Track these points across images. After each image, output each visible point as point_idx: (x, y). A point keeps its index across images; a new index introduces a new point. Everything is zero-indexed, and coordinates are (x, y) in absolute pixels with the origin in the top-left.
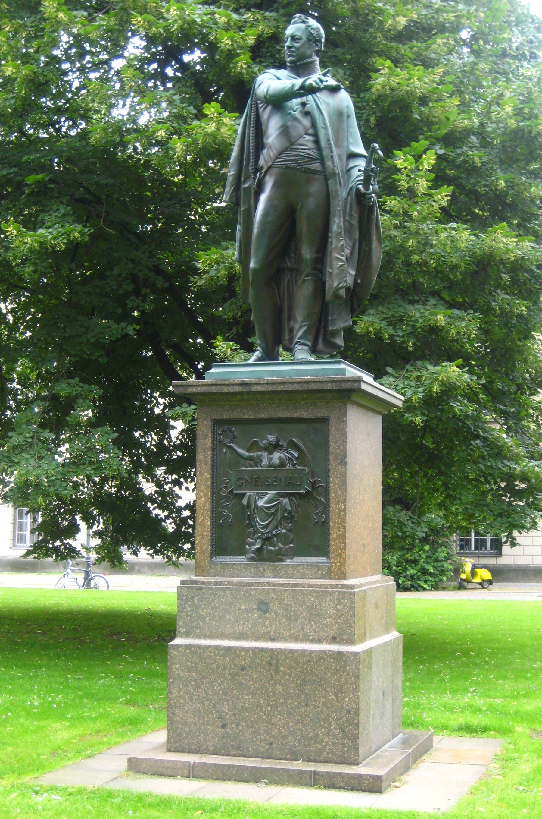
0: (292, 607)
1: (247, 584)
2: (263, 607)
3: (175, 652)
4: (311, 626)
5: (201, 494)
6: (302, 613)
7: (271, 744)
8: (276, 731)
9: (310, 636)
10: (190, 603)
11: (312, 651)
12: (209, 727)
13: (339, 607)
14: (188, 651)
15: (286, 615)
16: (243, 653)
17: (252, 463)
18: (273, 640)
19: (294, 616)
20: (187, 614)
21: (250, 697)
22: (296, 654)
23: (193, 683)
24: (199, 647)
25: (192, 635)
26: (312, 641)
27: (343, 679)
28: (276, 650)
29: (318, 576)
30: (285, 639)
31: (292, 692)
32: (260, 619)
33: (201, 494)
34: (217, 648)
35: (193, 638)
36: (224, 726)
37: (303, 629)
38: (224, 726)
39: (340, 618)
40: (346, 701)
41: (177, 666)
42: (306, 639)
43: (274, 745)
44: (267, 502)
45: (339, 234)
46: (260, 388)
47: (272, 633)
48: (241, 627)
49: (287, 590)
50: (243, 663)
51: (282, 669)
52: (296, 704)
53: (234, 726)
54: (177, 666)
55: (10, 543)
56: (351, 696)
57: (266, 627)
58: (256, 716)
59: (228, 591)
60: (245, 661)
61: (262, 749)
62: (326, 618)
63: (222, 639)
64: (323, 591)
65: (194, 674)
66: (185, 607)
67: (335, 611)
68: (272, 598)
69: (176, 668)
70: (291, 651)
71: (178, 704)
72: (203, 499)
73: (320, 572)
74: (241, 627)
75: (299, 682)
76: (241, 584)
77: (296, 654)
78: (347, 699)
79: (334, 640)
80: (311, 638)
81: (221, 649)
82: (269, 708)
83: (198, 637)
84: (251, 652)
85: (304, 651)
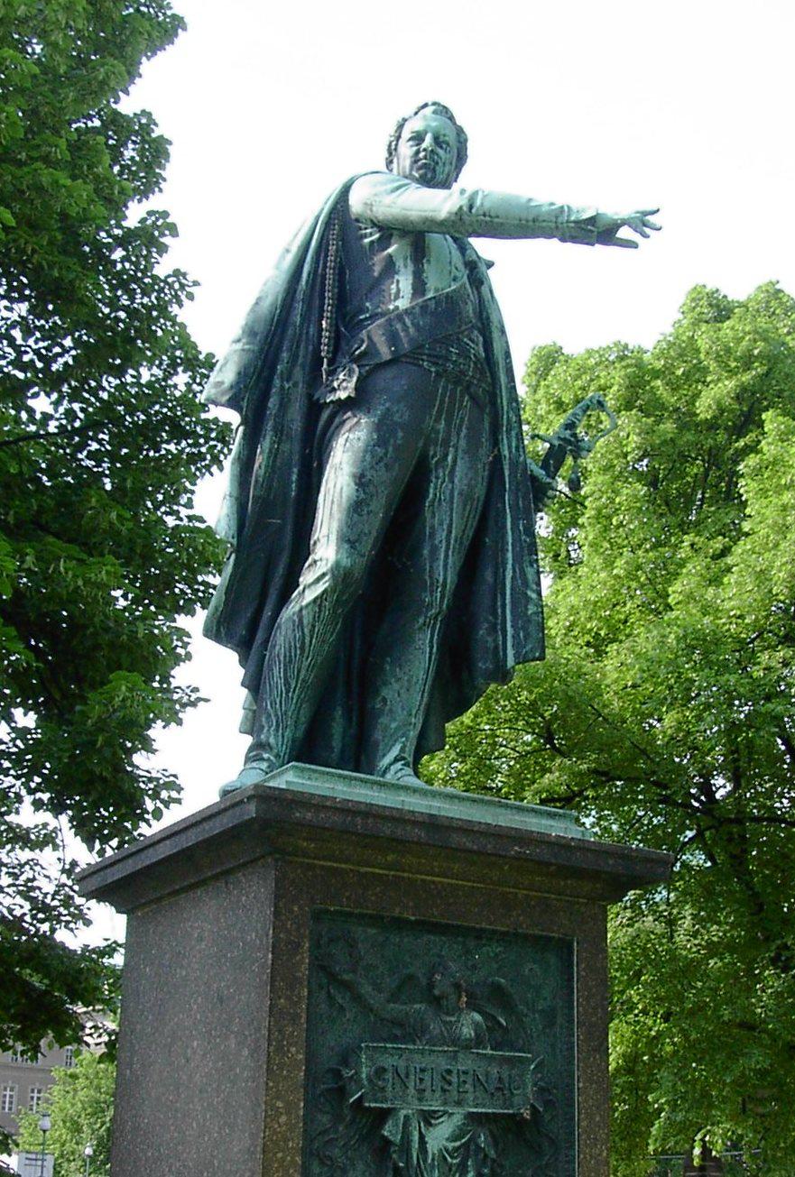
44: (453, 1138)
72: (283, 1119)
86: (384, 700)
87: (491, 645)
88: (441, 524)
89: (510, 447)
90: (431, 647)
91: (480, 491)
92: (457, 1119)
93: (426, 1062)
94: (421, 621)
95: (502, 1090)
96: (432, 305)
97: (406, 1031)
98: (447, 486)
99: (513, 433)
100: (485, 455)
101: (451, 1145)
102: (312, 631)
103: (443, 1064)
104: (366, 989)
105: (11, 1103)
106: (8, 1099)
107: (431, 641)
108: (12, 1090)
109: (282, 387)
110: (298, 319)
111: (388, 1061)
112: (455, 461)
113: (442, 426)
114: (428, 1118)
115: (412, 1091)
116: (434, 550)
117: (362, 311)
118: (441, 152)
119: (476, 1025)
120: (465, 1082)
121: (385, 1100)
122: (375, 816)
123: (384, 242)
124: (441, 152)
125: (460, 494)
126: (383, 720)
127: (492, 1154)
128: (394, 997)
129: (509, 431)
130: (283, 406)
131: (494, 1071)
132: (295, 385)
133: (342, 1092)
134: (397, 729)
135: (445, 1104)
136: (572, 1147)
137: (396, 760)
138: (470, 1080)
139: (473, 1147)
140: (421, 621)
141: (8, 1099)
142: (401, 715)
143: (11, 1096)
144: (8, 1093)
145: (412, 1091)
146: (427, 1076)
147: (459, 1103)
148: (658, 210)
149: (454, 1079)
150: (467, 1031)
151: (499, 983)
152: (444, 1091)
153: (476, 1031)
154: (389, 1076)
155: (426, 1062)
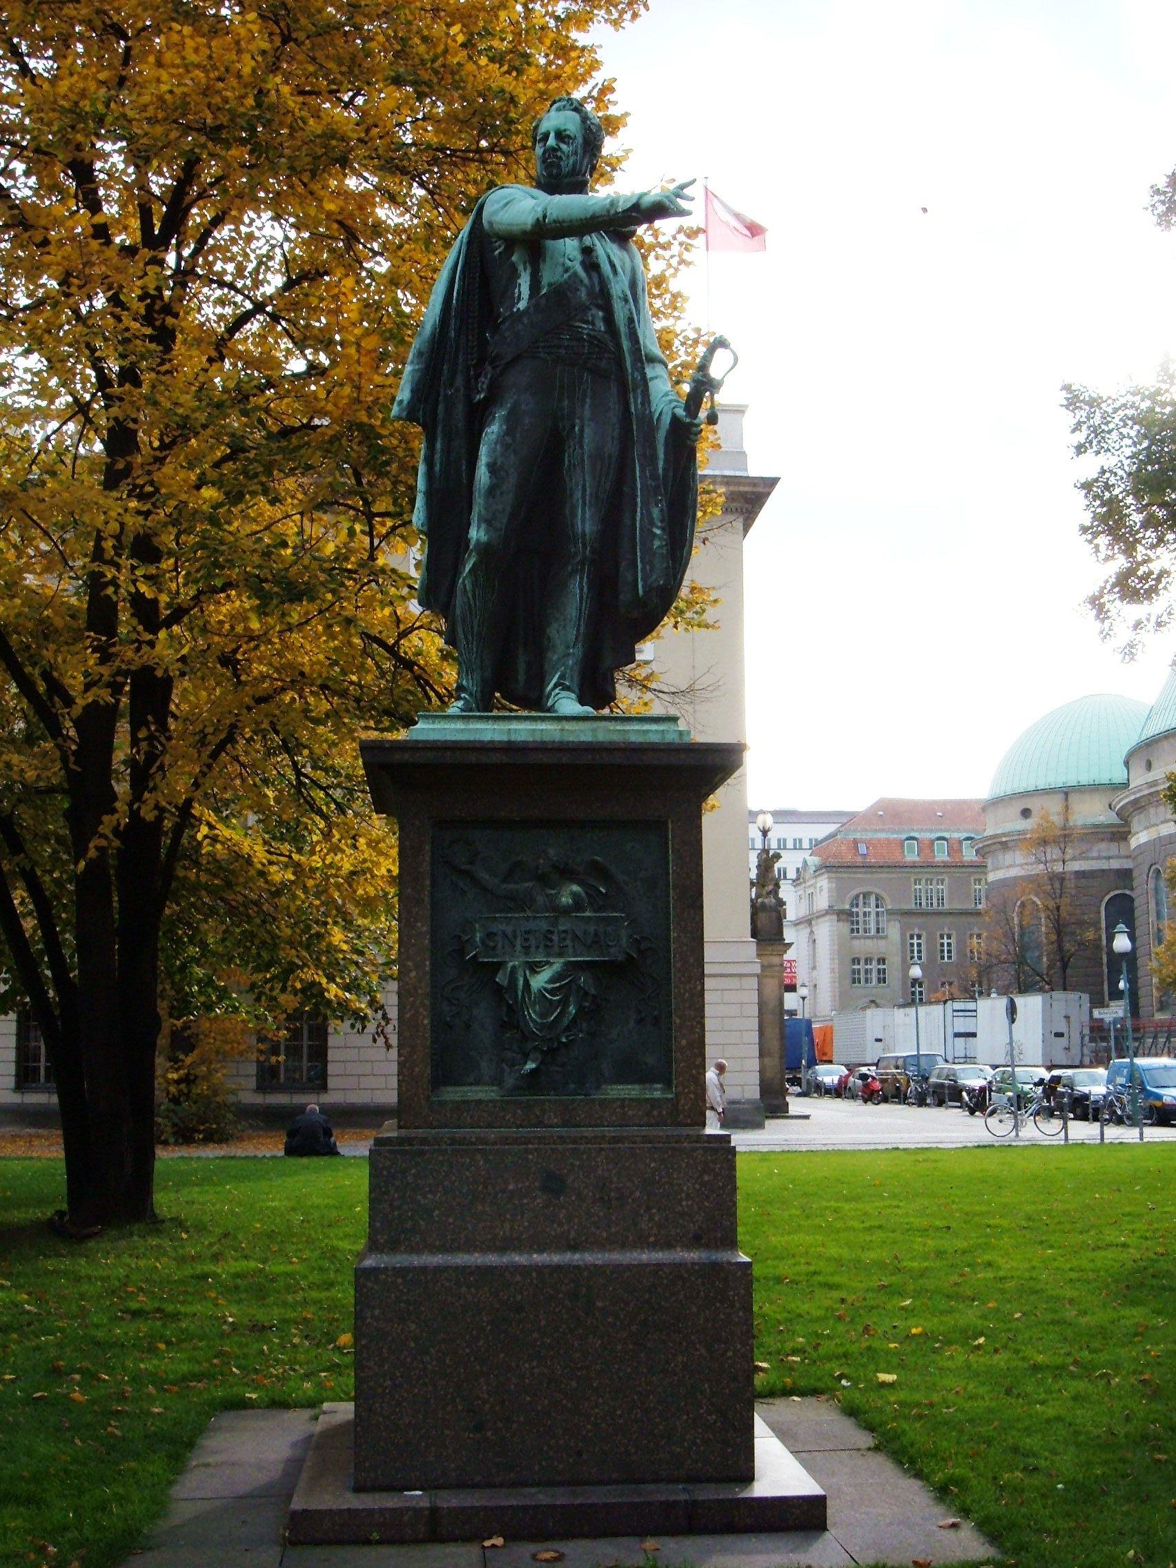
0: (611, 1182)
1: (516, 1141)
2: (553, 1184)
3: (370, 1285)
4: (651, 1219)
5: (410, 963)
6: (632, 1193)
7: (579, 1454)
8: (589, 1427)
9: (649, 1236)
10: (397, 1183)
11: (660, 1266)
12: (447, 1432)
13: (706, 1178)
14: (399, 1281)
15: (602, 1198)
16: (518, 1278)
17: (511, 904)
18: (574, 1248)
19: (617, 1199)
20: (391, 1205)
21: (535, 1363)
22: (627, 1274)
23: (412, 1345)
24: (424, 1269)
25: (403, 1248)
26: (654, 1246)
27: (722, 1316)
28: (587, 1267)
29: (653, 1121)
30: (602, 1246)
31: (619, 1347)
32: (547, 1207)
33: (410, 963)
34: (463, 1270)
35: (406, 1252)
36: (479, 1427)
37: (635, 1224)
38: (479, 1427)
39: (707, 1197)
40: (729, 1358)
41: (377, 1312)
42: (642, 1242)
43: (585, 1457)
44: (551, 981)
45: (158, 568)
46: (545, 759)
47: (573, 1234)
48: (507, 1225)
49: (602, 1149)
50: (519, 1297)
51: (600, 1304)
52: (629, 1370)
53: (500, 1425)
54: (377, 1312)
55: (11, 1081)
56: (739, 1346)
57: (561, 1224)
58: (546, 1401)
59: (478, 1157)
60: (521, 1293)
61: (561, 1466)
62: (681, 1200)
63: (468, 1252)
64: (674, 1149)
65: (413, 1327)
66: (387, 1193)
67: (697, 1186)
68: (572, 1165)
69: (373, 1317)
70: (619, 1268)
71: (380, 1390)
72: (413, 974)
73: (655, 1113)
74: (507, 1225)
75: (634, 1328)
76: (505, 1141)
77: (627, 1274)
78: (730, 1354)
79: (696, 1241)
80: (652, 1239)
81: (471, 1273)
82: (574, 1384)
83: (415, 1250)
84: (534, 1275)
85: (643, 1266)
86: (549, 639)
87: (630, 578)
88: (577, 485)
89: (636, 402)
90: (581, 590)
91: (611, 448)
92: (558, 965)
93: (531, 925)
94: (570, 568)
95: (596, 943)
96: (543, 301)
97: (520, 903)
98: (578, 451)
99: (639, 391)
100: (613, 416)
101: (550, 986)
102: (474, 595)
103: (544, 926)
104: (483, 875)
105: (949, 951)
106: (946, 948)
107: (581, 583)
108: (949, 937)
109: (446, 395)
110: (452, 334)
111: (499, 927)
112: (582, 430)
113: (566, 403)
114: (534, 968)
115: (518, 947)
116: (574, 508)
117: (499, 317)
118: (564, 147)
119: (574, 895)
120: (564, 939)
121: (496, 956)
122: (461, 749)
123: (509, 251)
124: (564, 147)
125: (590, 457)
126: (549, 654)
127: (593, 991)
128: (504, 881)
129: (634, 390)
130: (448, 411)
131: (592, 929)
132: (457, 390)
133: (461, 952)
134: (559, 659)
135: (548, 955)
136: (669, 984)
137: (555, 686)
138: (569, 937)
139: (574, 986)
140: (570, 568)
141: (946, 948)
142: (561, 649)
143: (949, 945)
144: (945, 941)
145: (518, 947)
146: (531, 937)
147: (560, 955)
148: (694, 181)
149: (555, 938)
150: (566, 900)
151: (597, 862)
152: (546, 946)
153: (574, 900)
154: (499, 938)
155: (531, 925)
